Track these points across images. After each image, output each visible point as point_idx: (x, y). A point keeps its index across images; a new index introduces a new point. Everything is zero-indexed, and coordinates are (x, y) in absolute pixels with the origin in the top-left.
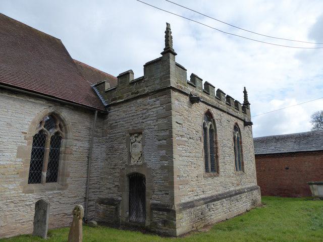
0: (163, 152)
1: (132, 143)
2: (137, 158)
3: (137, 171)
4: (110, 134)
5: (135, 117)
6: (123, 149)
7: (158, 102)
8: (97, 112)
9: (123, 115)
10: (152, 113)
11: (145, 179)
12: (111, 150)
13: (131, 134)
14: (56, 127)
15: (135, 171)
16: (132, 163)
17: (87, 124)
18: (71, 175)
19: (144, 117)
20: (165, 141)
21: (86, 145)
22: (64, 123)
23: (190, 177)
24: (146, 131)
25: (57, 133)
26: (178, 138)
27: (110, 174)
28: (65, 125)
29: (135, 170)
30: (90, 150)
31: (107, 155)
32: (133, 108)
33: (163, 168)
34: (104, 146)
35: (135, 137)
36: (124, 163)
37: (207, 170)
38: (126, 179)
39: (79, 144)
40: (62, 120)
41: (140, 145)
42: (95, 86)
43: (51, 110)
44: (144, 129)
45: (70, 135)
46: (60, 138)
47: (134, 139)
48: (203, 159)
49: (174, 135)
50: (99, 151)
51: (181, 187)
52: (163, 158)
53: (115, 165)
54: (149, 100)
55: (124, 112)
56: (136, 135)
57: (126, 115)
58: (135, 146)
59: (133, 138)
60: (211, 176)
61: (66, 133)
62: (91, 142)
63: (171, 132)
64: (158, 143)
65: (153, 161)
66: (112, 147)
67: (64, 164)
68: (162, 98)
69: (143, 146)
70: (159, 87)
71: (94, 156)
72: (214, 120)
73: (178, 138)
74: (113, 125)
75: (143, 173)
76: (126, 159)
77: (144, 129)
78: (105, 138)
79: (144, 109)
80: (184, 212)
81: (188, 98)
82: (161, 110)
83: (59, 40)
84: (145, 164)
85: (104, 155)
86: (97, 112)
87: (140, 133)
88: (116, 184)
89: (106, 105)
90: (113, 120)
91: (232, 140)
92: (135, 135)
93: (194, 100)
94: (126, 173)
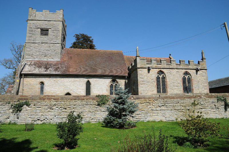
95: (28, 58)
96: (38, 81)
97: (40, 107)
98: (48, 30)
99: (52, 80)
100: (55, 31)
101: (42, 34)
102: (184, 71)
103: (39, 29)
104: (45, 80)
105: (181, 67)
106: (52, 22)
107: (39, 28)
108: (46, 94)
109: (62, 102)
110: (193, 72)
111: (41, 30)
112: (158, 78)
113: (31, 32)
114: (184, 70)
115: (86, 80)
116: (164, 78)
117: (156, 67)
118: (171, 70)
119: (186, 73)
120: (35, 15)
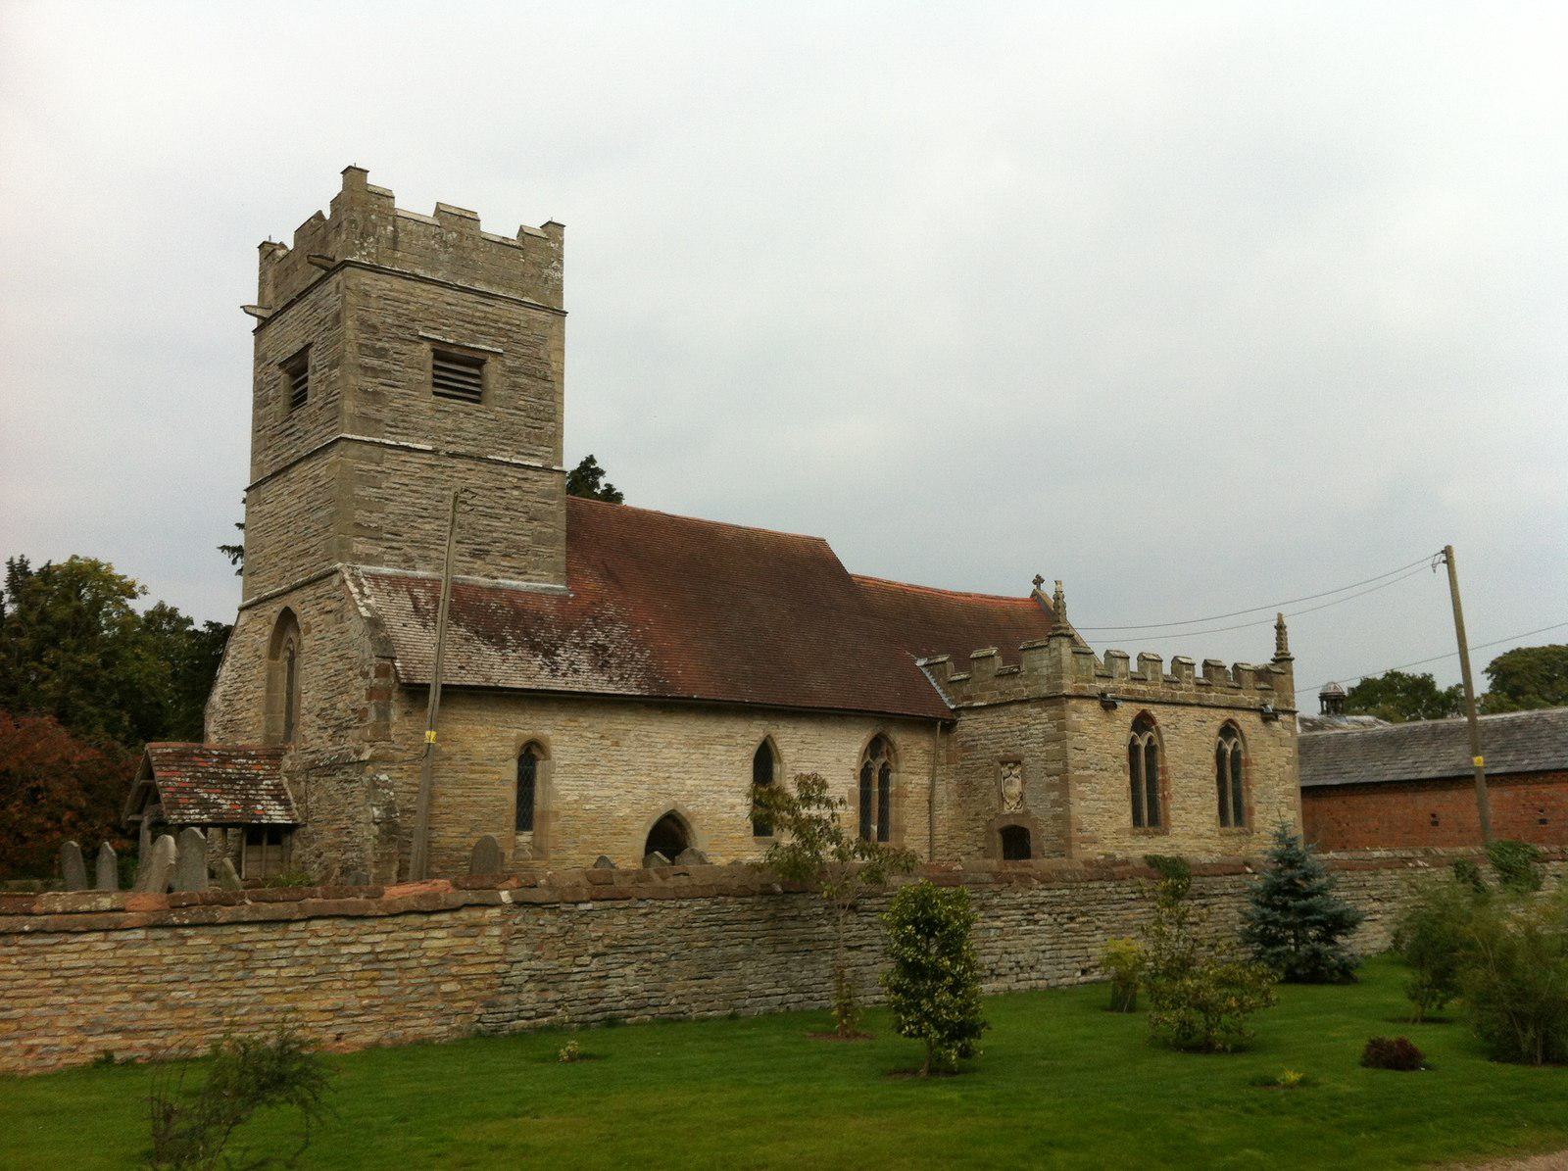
0: (1055, 795)
1: (1004, 778)
2: (1013, 803)
3: (1016, 824)
4: (963, 759)
5: (1006, 735)
6: (989, 788)
7: (1044, 715)
8: (939, 723)
9: (987, 729)
10: (1037, 730)
11: (1028, 833)
12: (967, 789)
13: (1003, 763)
14: (882, 756)
15: (1013, 823)
16: (1006, 810)
17: (925, 744)
18: (909, 830)
19: (1023, 736)
20: (1056, 778)
21: (926, 780)
22: (893, 748)
23: (1100, 833)
24: (1029, 759)
25: (884, 765)
26: (1077, 773)
27: (968, 830)
28: (895, 751)
29: (1012, 822)
30: (932, 787)
31: (960, 796)
32: (1004, 720)
33: (1055, 818)
34: (952, 781)
35: (1010, 768)
36: (992, 810)
37: (1137, 819)
38: (998, 836)
39: (915, 779)
40: (891, 744)
41: (1018, 782)
42: (925, 666)
43: (879, 730)
44: (1023, 757)
45: (903, 766)
46: (888, 771)
47: (1008, 772)
48: (1128, 804)
49: (1070, 768)
50: (945, 790)
51: (1083, 846)
52: (1055, 803)
53: (977, 814)
54: (1030, 710)
55: (987, 723)
56: (1012, 765)
57: (991, 729)
58: (1011, 783)
59: (1005, 770)
60: (1146, 833)
61: (897, 762)
62: (933, 775)
63: (1066, 764)
64: (1047, 780)
65: (1041, 812)
66: (969, 783)
67: (897, 812)
68: (1052, 711)
69: (1024, 783)
70: (1045, 691)
71: (937, 798)
72: (1157, 728)
73: (1077, 773)
74: (967, 744)
75: (1026, 825)
76: (995, 803)
77: (1023, 757)
78: (953, 766)
79: (1022, 724)
80: (1110, 996)
81: (1097, 704)
82: (1051, 728)
83: (822, 541)
84: (1027, 813)
85: (954, 797)
86: (939, 723)
87: (1018, 763)
88: (980, 845)
89: (953, 707)
90: (967, 735)
91: (1212, 760)
92: (1009, 765)
93: (1108, 705)
94: (997, 825)
95: (369, 559)
96: (514, 734)
97: (999, 917)
98: (480, 364)
99: (591, 727)
100: (523, 380)
101: (444, 387)
102: (1222, 716)
103: (426, 346)
104: (549, 728)
105: (1212, 696)
106: (501, 304)
107: (428, 339)
108: (1094, 852)
109: (1064, 891)
110: (1248, 722)
111: (438, 355)
112: (1133, 749)
113: (376, 362)
114: (1223, 712)
115: (749, 734)
116: (1151, 750)
117: (1128, 691)
118: (1178, 709)
119: (1228, 730)
120: (390, 228)
